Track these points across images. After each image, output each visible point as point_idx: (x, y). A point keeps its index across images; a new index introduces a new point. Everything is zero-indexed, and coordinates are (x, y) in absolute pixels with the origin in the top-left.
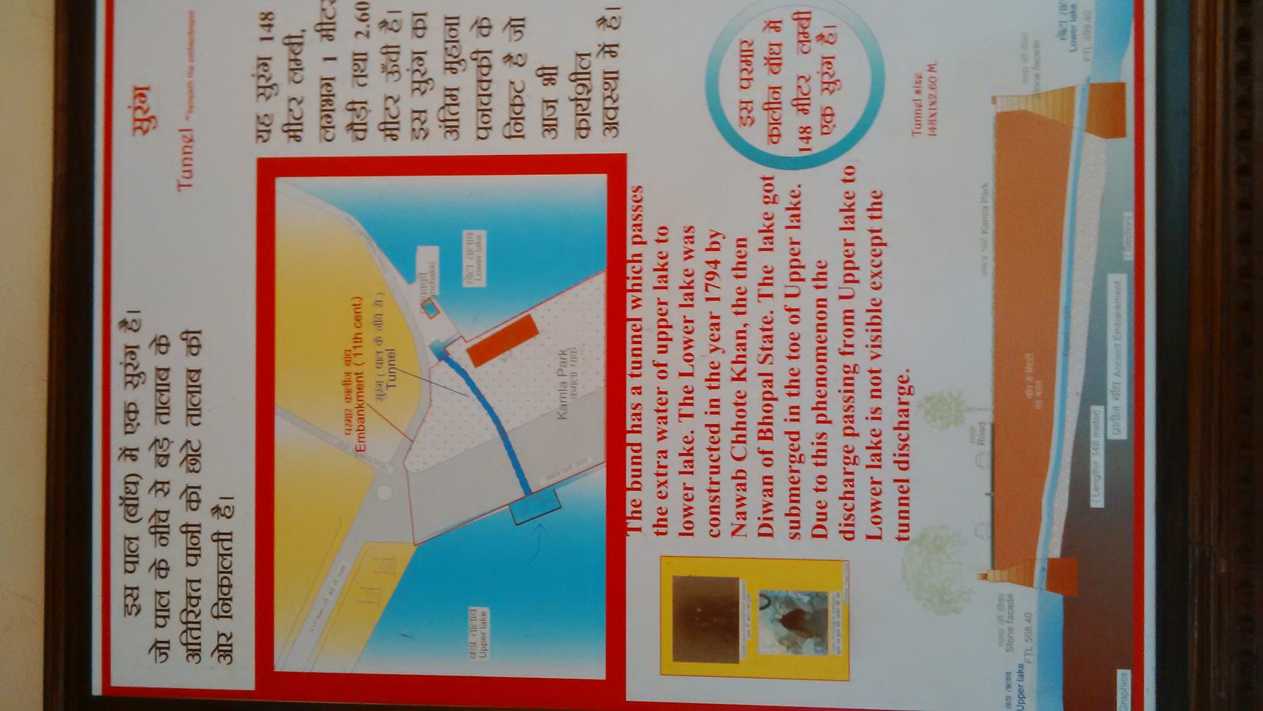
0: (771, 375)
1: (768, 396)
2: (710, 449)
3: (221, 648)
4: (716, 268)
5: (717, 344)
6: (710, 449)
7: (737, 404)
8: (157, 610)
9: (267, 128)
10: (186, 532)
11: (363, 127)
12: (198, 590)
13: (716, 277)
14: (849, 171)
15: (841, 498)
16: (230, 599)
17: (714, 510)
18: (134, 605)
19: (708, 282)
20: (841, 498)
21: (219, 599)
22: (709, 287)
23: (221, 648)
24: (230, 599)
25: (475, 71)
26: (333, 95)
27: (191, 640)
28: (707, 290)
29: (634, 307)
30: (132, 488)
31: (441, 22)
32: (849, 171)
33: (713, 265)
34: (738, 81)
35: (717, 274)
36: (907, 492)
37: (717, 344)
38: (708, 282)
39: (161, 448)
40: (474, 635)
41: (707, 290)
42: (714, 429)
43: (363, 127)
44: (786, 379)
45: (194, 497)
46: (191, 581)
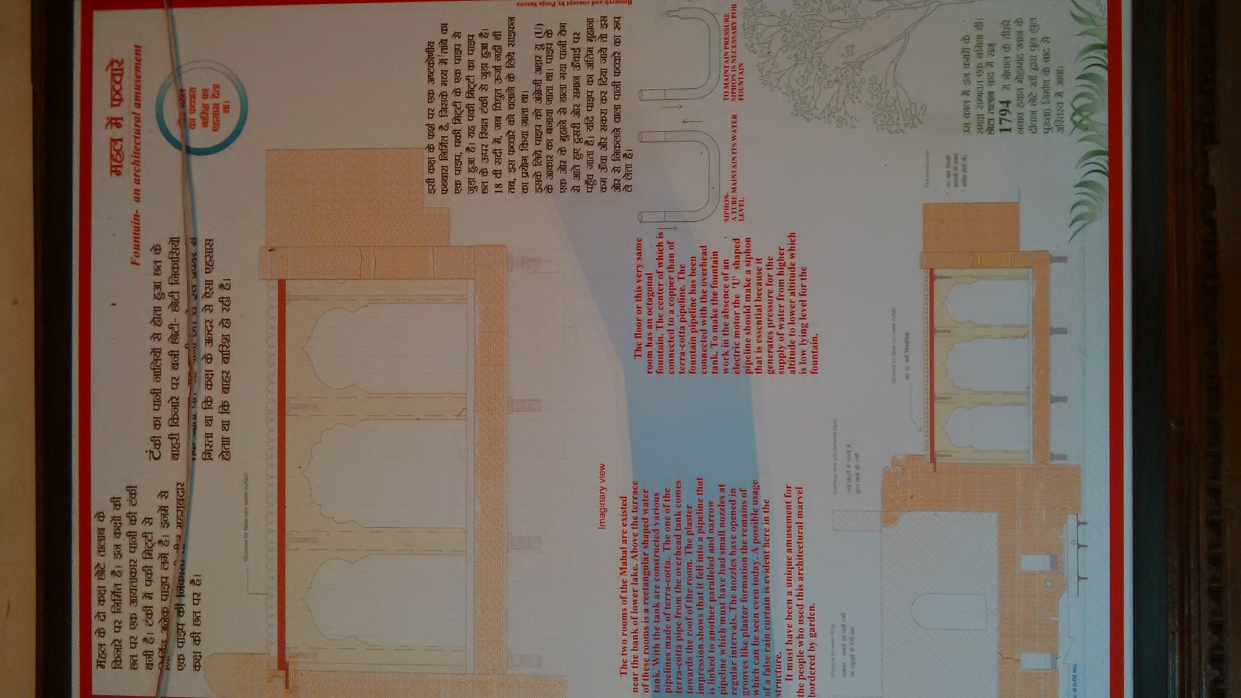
0: (760, 306)
2: (702, 341)
4: (1007, 106)
6: (702, 341)
7: (735, 323)
8: (130, 544)
9: (104, 660)
10: (536, 83)
12: (211, 441)
13: (1008, 113)
16: (178, 275)
17: (671, 362)
18: (177, 443)
19: (1001, 117)
21: (173, 275)
22: (1003, 121)
24: (178, 275)
27: (589, 59)
28: (1000, 123)
33: (1006, 104)
35: (1009, 112)
36: (772, 357)
38: (1001, 117)
41: (1000, 123)
42: (704, 332)
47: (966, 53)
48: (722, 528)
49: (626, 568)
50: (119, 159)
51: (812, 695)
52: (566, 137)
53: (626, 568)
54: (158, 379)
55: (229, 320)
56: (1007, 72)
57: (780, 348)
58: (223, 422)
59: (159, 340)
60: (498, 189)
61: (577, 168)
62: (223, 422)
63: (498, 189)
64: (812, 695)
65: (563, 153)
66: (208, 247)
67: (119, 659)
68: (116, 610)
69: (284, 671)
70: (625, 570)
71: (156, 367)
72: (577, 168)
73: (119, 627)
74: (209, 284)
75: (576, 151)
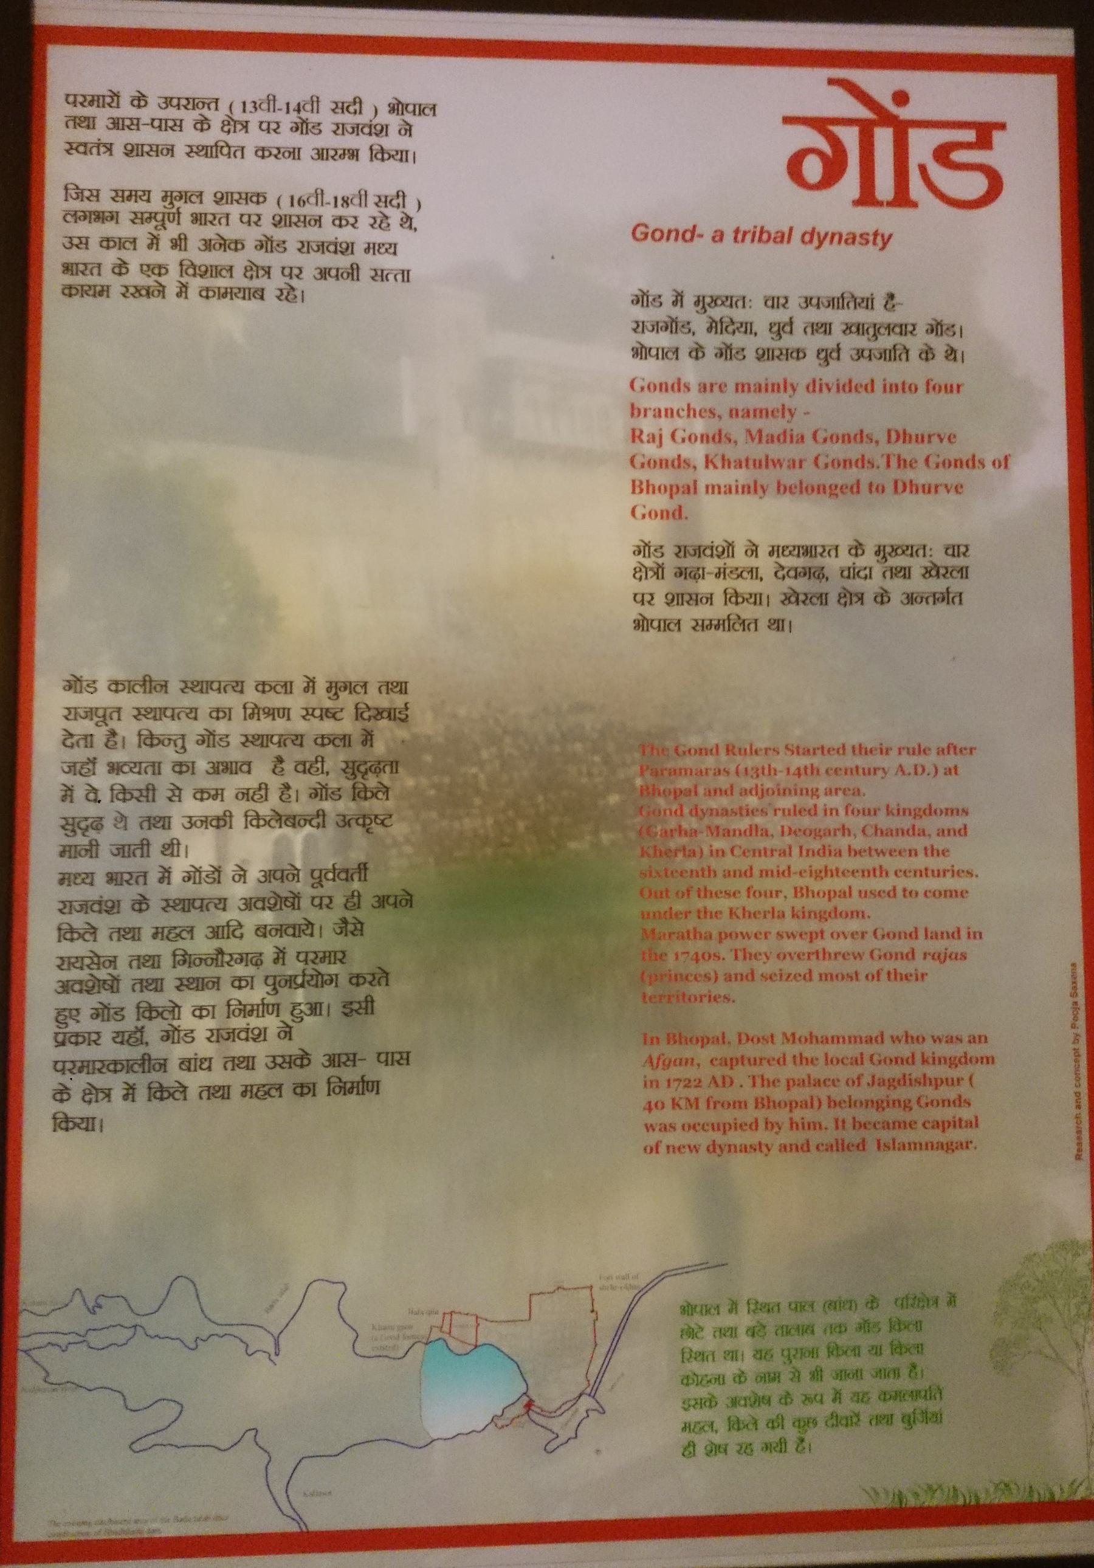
1: (674, 489)
3: (884, 138)
5: (946, 440)
11: (272, 109)
14: (913, 388)
15: (689, 405)
20: (689, 405)
23: (884, 138)
25: (288, 145)
26: (801, 483)
27: (898, 353)
29: (749, 431)
30: (206, 1065)
31: (297, 145)
32: (913, 388)
34: (73, 92)
37: (946, 440)
39: (942, 154)
40: (805, 332)
43: (272, 109)
44: (807, 1054)
45: (690, 1381)
46: (145, 876)
47: (108, 100)
48: (703, 490)
49: (760, 441)
50: (172, 936)
51: (782, 488)
52: (884, 557)
53: (760, 441)
54: (240, 796)
55: (266, 800)
56: (803, 1308)
57: (790, 410)
58: (160, 763)
59: (333, 110)
60: (340, 202)
61: (904, 356)
62: (160, 763)
63: (340, 202)
64: (782, 488)
65: (136, 103)
66: (147, 149)
67: (386, 156)
68: (332, 1086)
69: (974, 140)
70: (757, 440)
71: (231, 929)
72: (904, 356)
73: (178, 105)
74: (366, 1008)
75: (74, 1013)
